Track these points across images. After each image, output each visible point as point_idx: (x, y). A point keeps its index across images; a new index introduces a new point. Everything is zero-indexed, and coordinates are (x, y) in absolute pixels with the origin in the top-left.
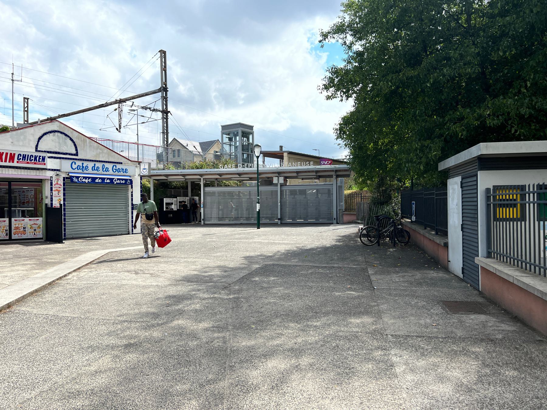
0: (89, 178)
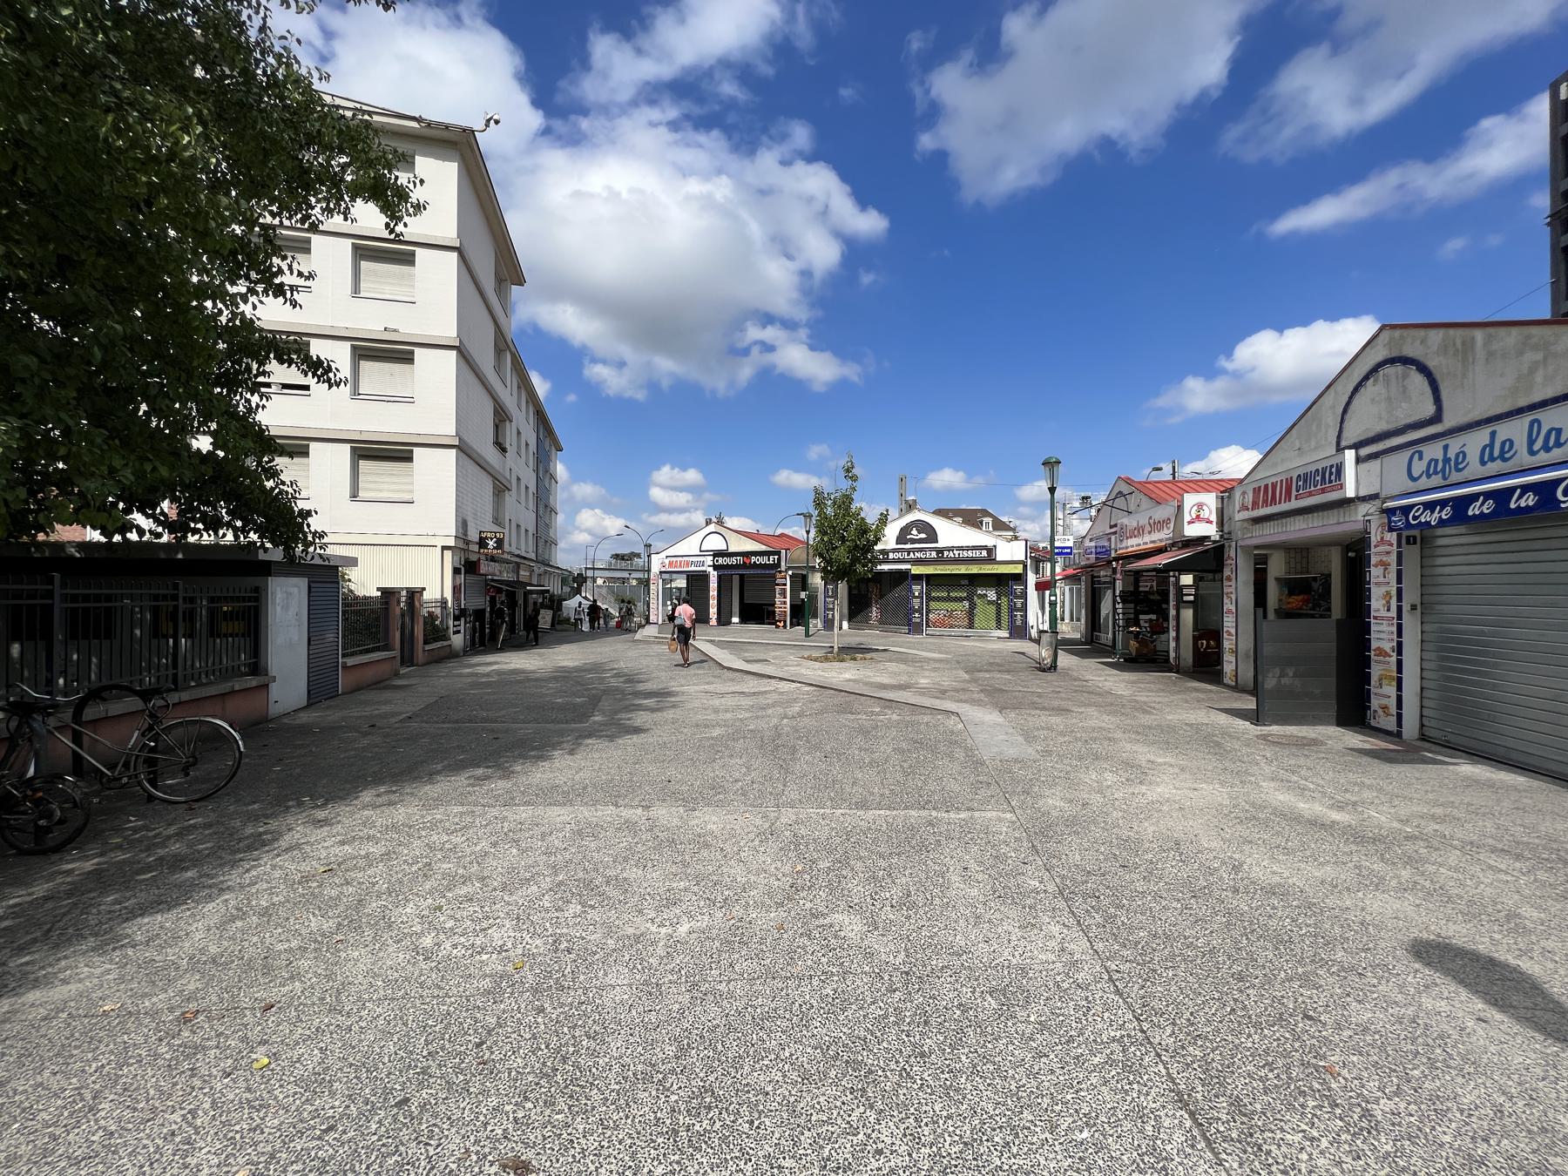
0: (1443, 503)
